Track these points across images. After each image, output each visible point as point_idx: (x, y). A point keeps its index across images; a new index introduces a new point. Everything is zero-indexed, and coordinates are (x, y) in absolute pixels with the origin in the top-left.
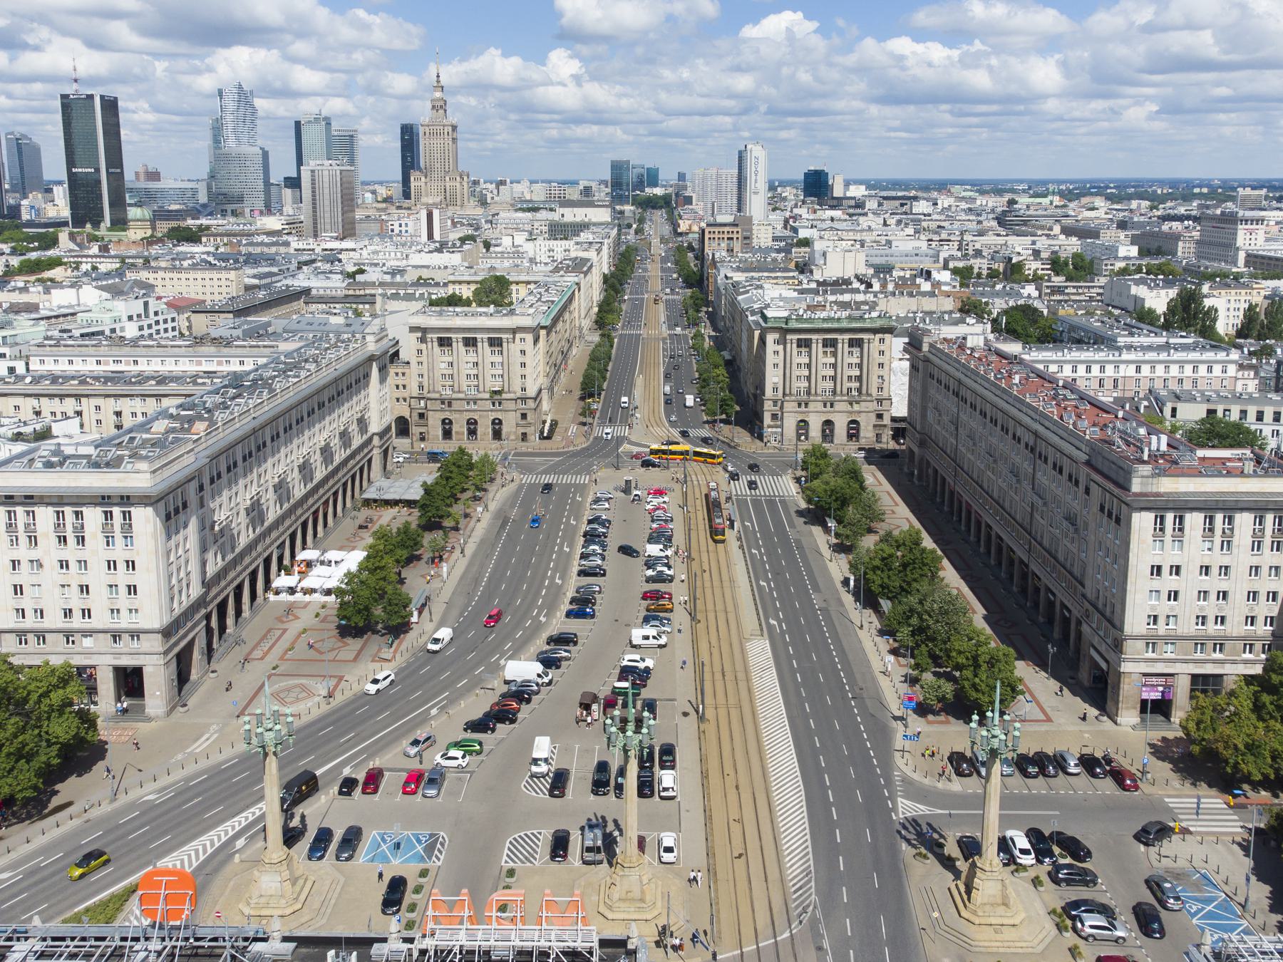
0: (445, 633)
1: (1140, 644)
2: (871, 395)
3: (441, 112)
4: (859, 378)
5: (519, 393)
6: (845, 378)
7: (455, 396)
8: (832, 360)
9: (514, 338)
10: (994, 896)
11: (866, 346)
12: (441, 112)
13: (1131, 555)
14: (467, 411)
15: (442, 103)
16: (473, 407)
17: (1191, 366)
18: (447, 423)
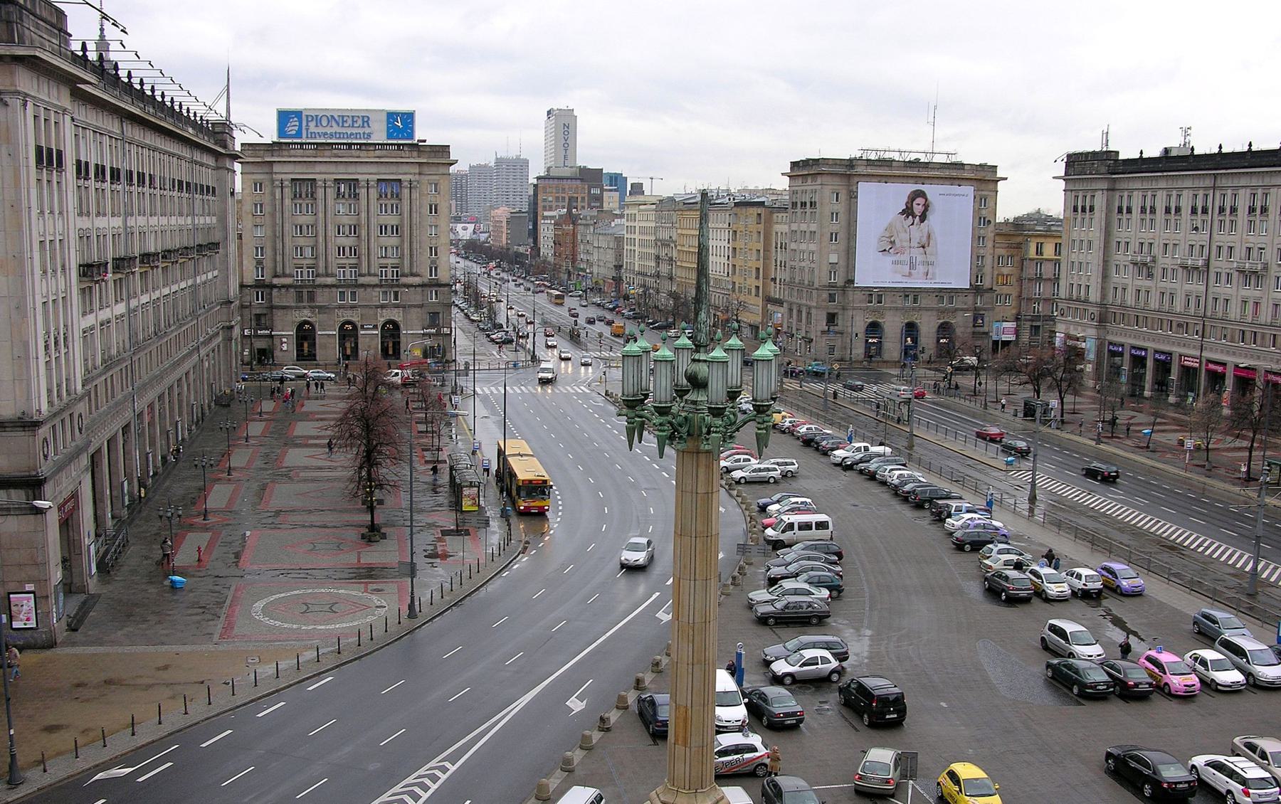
0: (522, 508)
4: (355, 229)
5: (427, 277)
7: (320, 280)
17: (1191, 193)
18: (305, 335)
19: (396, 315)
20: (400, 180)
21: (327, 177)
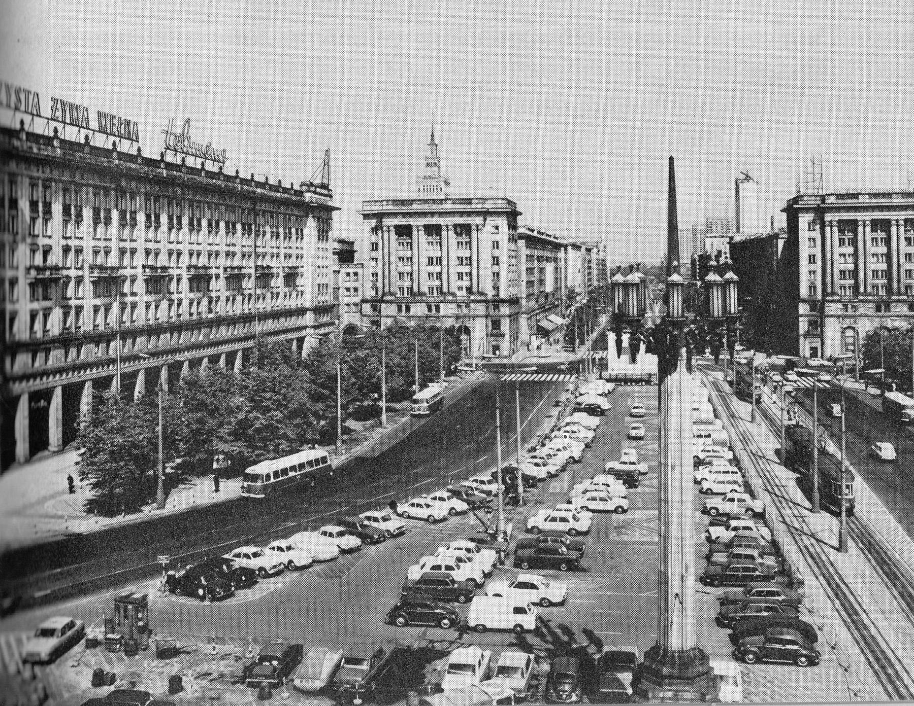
6: (837, 275)
11: (474, 233)
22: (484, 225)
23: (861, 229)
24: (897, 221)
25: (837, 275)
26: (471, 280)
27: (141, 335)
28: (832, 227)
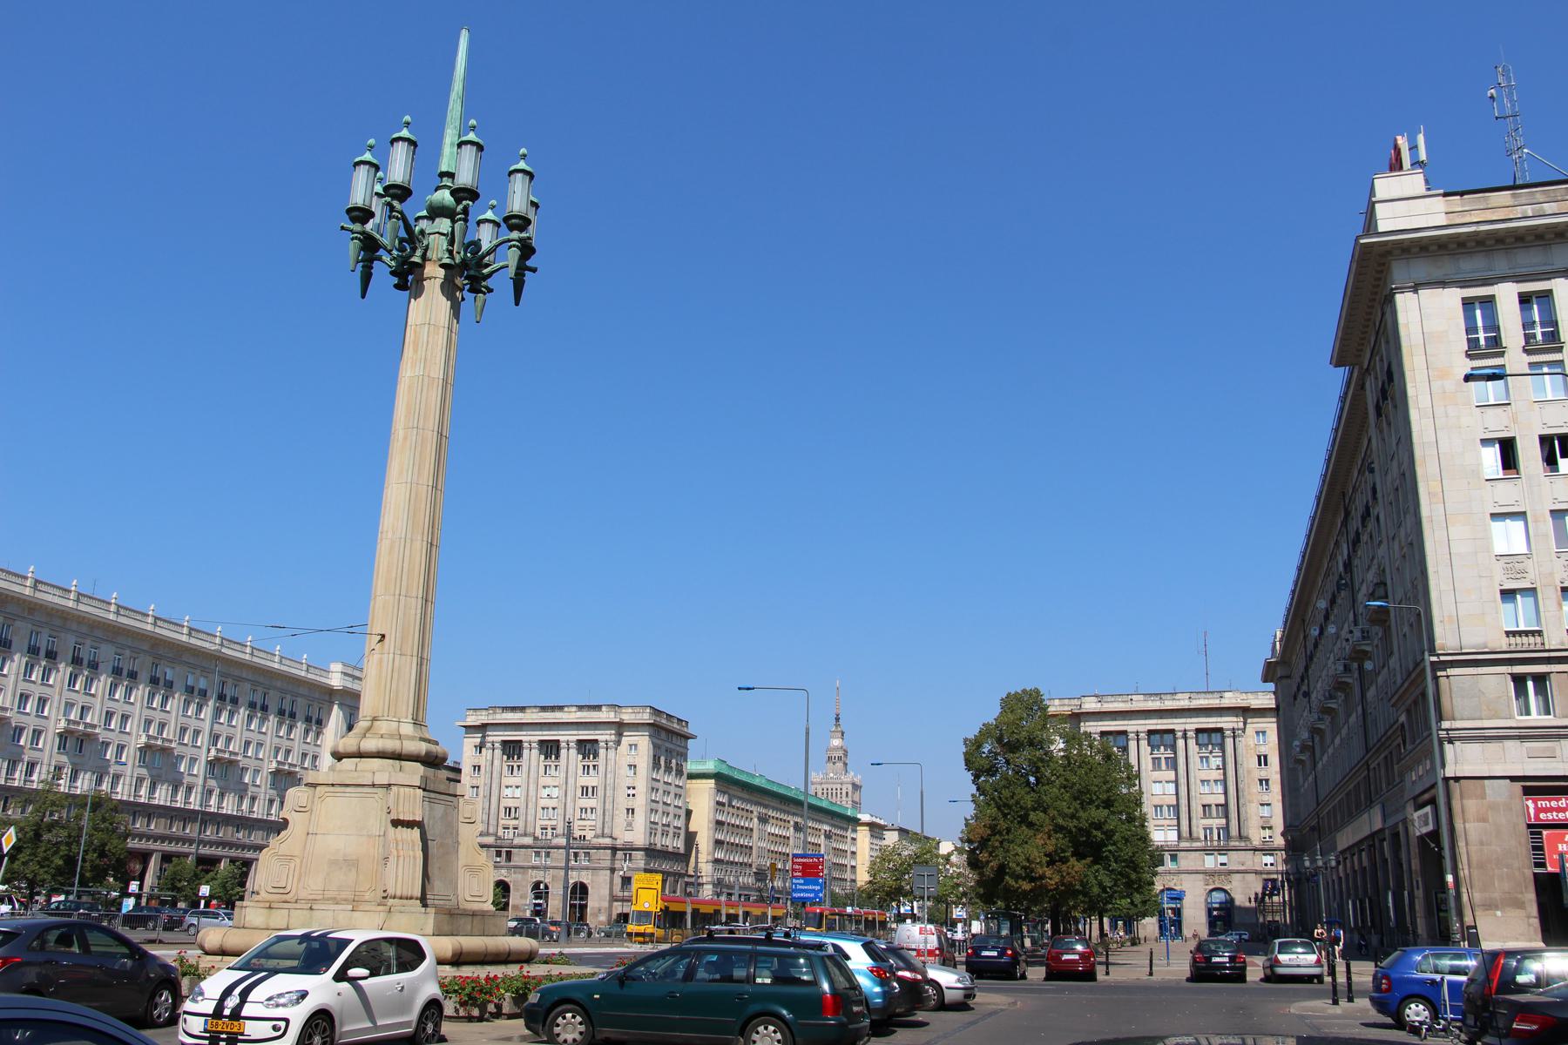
1: (1497, 682)
2: (1247, 839)
3: (840, 765)
6: (1197, 810)
7: (517, 841)
8: (1171, 775)
9: (618, 743)
10: (352, 863)
11: (1229, 742)
12: (840, 765)
13: (1414, 415)
14: (533, 868)
15: (840, 753)
16: (542, 861)
19: (585, 877)
20: (596, 741)
21: (532, 738)
22: (1244, 730)
23: (1181, 743)
24: (1137, 733)
25: (1197, 810)
26: (1227, 817)
27: (160, 816)
28: (1185, 737)
